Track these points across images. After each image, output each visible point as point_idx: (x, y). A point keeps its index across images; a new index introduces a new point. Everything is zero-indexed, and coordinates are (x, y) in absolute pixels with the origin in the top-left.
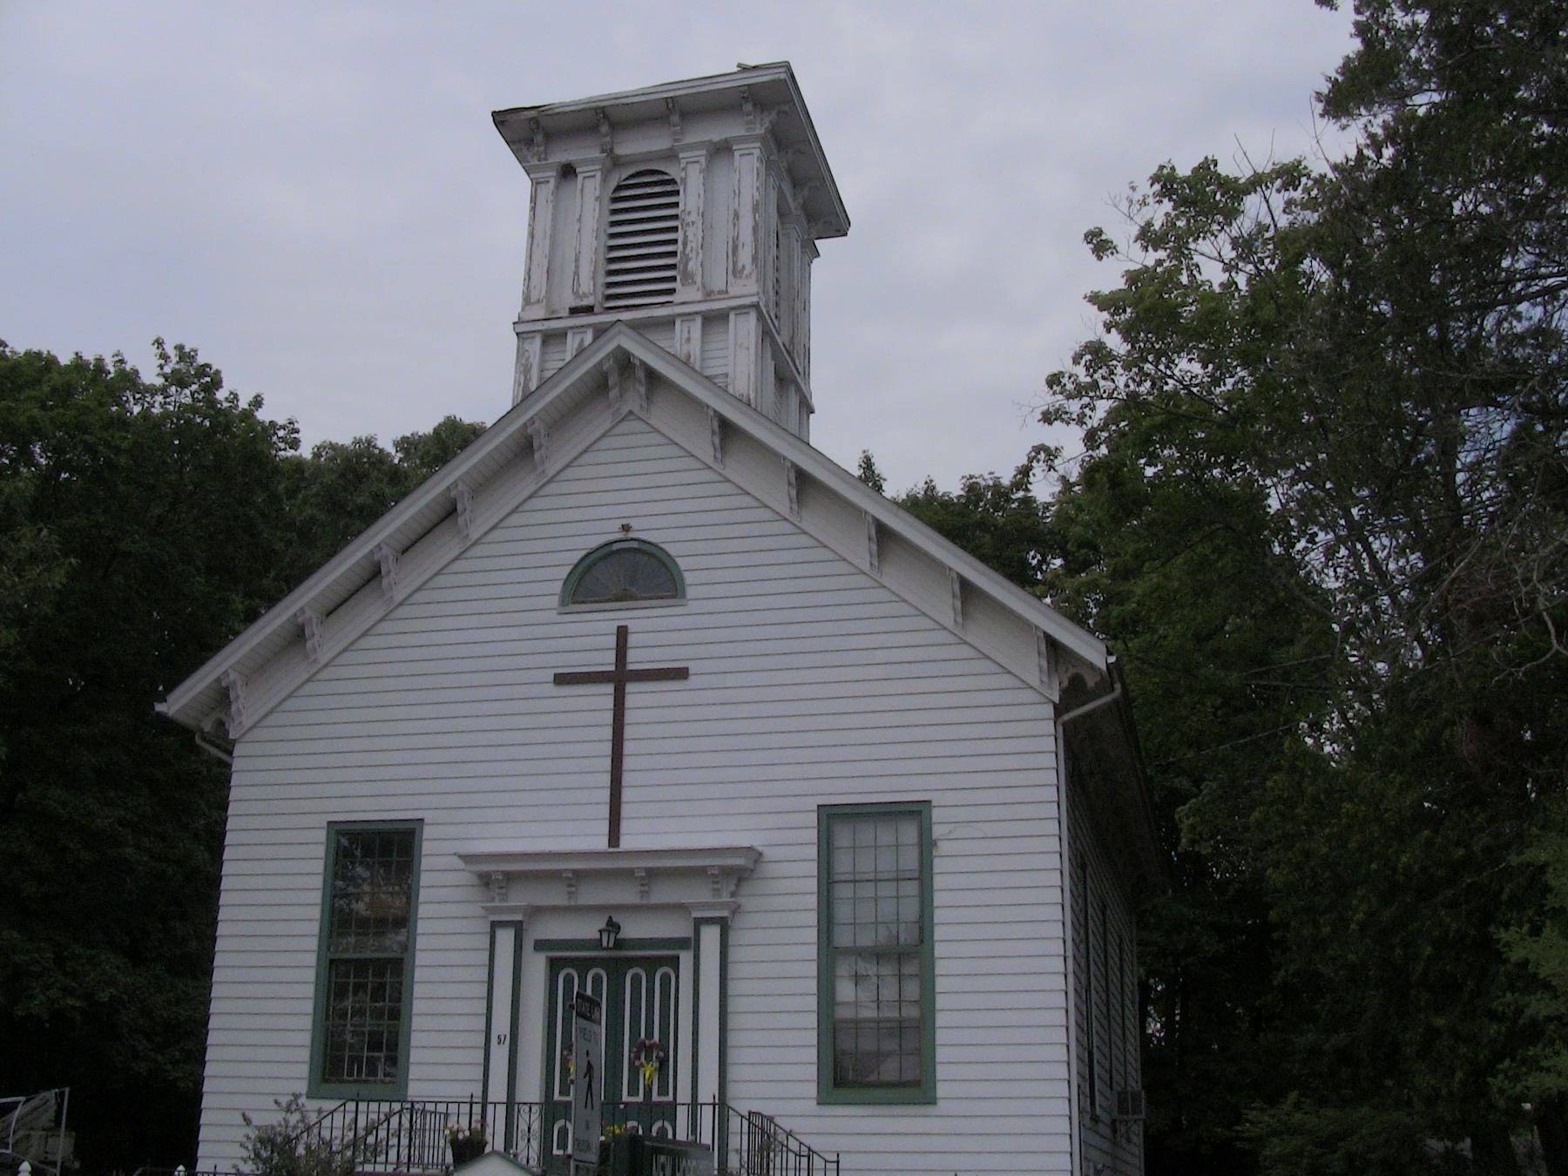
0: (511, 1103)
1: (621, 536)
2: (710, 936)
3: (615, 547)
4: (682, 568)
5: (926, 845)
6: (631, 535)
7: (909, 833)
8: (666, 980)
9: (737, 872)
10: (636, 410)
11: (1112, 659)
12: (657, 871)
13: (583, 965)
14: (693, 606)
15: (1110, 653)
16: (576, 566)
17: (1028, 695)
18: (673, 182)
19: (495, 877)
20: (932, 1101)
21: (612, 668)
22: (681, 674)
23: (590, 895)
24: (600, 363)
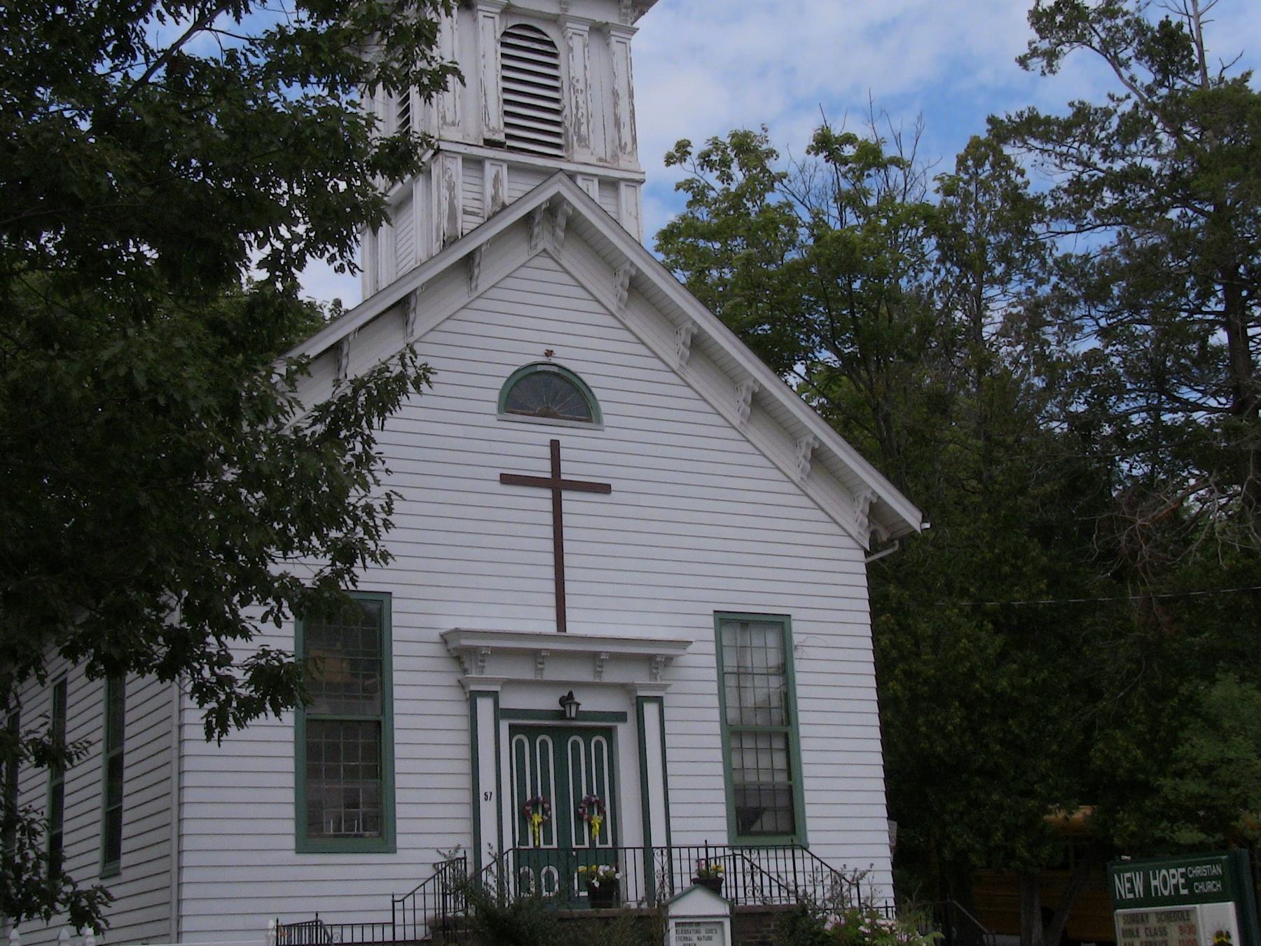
0: (648, 850)
1: (545, 359)
2: (650, 711)
3: (540, 368)
4: (598, 397)
5: (786, 648)
6: (554, 361)
7: (772, 638)
8: (599, 746)
9: (656, 659)
10: (550, 249)
11: (927, 526)
12: (595, 655)
13: (532, 732)
14: (608, 432)
15: (924, 520)
16: (509, 379)
17: (847, 542)
18: (551, 44)
19: (462, 652)
20: (392, 850)
21: (549, 476)
22: (605, 489)
23: (553, 672)
24: (569, 204)
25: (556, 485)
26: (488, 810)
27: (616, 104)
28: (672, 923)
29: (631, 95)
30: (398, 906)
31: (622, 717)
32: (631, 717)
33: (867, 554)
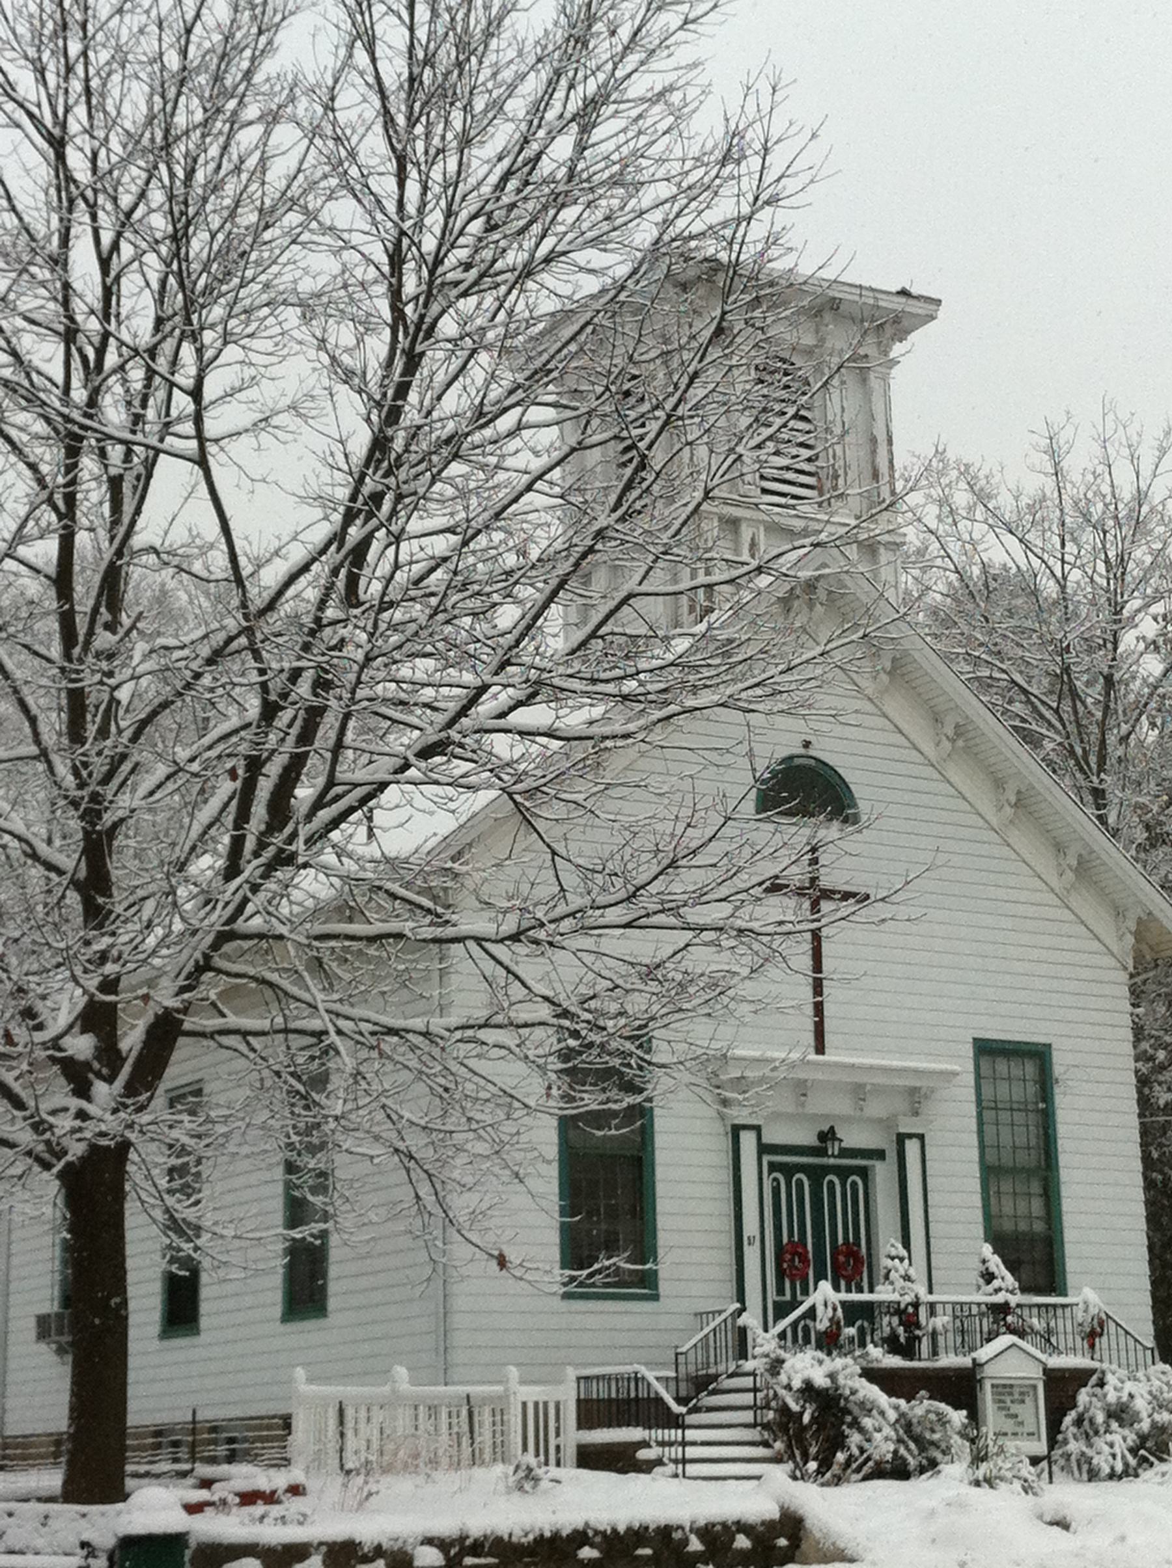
1: (802, 751)
2: (912, 1147)
3: (797, 761)
6: (812, 753)
7: (1030, 1069)
13: (788, 1171)
25: (817, 894)
26: (752, 1256)
27: (874, 452)
28: (987, 1385)
29: (890, 442)
30: (681, 1359)
31: (880, 1154)
32: (891, 1155)
33: (1132, 976)
